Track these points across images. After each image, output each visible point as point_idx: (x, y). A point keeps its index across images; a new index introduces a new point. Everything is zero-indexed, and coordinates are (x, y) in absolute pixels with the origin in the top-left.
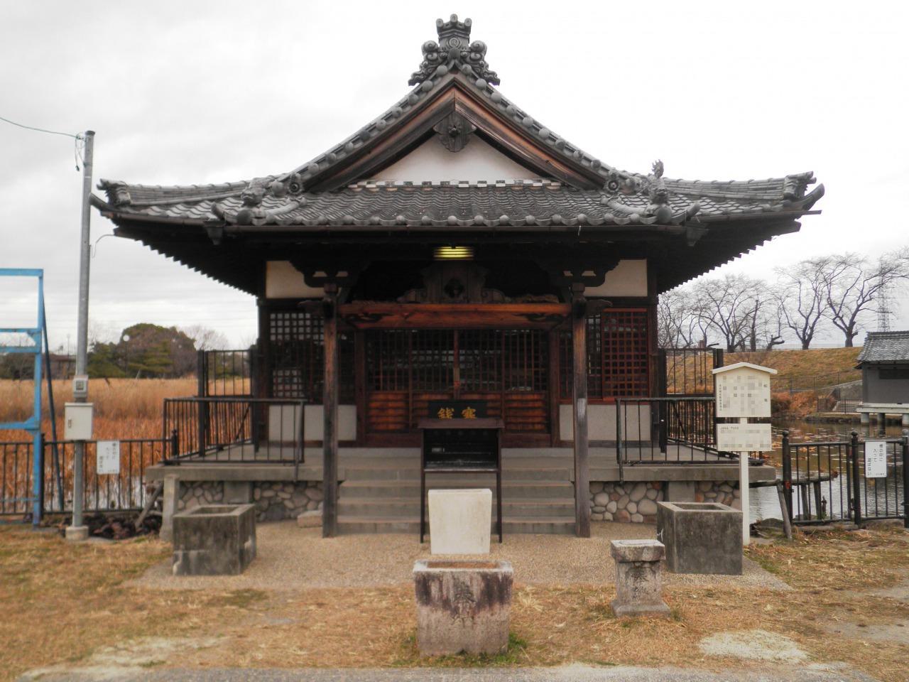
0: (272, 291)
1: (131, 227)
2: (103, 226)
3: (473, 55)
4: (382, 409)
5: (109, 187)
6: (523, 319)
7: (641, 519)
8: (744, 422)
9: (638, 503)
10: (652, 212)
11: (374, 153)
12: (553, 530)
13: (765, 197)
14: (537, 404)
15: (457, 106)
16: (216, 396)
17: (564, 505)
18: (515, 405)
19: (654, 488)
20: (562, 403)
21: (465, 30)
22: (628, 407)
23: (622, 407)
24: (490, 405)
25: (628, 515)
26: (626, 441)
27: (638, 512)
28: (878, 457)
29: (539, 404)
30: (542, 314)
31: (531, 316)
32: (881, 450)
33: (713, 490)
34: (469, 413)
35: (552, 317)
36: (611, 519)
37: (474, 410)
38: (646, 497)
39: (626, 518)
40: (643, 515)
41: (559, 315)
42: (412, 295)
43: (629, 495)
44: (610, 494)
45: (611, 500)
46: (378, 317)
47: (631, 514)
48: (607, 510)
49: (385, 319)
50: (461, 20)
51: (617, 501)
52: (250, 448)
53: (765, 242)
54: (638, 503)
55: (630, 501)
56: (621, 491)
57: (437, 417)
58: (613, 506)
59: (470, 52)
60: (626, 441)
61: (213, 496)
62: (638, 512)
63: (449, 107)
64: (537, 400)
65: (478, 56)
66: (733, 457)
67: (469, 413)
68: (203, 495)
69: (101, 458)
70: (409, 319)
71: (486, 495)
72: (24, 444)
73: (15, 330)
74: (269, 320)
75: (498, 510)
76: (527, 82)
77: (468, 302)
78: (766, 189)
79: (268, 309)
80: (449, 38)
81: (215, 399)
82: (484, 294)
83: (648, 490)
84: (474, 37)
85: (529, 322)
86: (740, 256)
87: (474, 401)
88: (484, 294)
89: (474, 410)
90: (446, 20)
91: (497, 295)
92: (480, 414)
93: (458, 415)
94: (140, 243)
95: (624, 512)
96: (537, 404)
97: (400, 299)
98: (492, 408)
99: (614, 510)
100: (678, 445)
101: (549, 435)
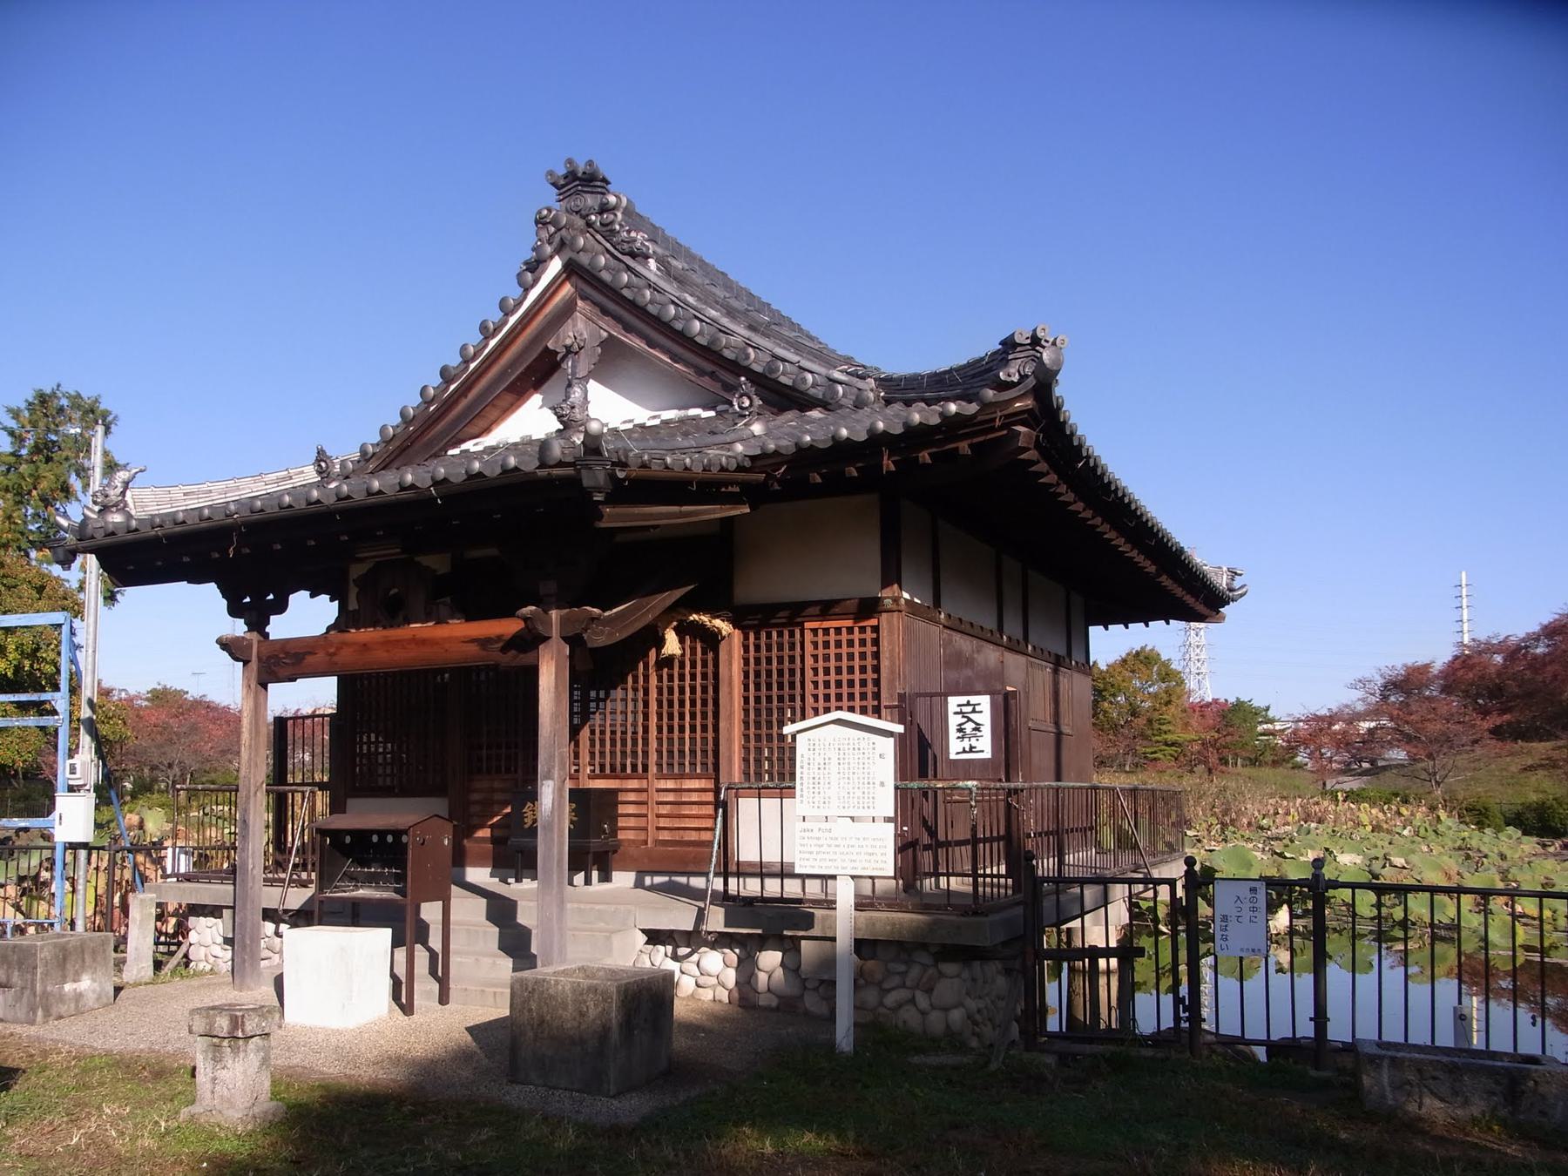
30: (499, 638)
90: (561, 171)
94: (181, 588)
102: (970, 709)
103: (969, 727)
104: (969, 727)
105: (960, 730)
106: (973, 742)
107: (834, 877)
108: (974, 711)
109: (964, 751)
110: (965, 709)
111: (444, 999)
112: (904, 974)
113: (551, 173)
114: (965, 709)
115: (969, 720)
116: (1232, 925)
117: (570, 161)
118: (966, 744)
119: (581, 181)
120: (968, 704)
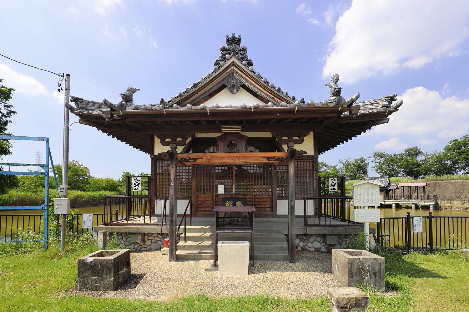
0: (156, 153)
1: (88, 119)
2: (74, 118)
3: (241, 52)
4: (204, 201)
5: (76, 100)
6: (265, 161)
7: (314, 250)
8: (367, 208)
9: (312, 243)
10: (332, 101)
11: (200, 93)
12: (277, 259)
13: (372, 108)
14: (267, 200)
15: (235, 75)
16: (134, 195)
17: (282, 246)
18: (258, 200)
19: (319, 236)
20: (278, 199)
21: (238, 41)
22: (309, 200)
23: (307, 201)
24: (248, 200)
25: (308, 248)
26: (308, 215)
27: (312, 247)
28: (419, 223)
29: (269, 200)
30: (274, 157)
31: (269, 158)
32: (420, 221)
33: (345, 237)
34: (239, 203)
35: (278, 159)
36: (301, 250)
37: (241, 202)
38: (316, 240)
39: (307, 249)
40: (315, 248)
41: (282, 158)
42: (212, 149)
43: (308, 239)
44: (300, 239)
45: (300, 242)
46: (195, 160)
47: (309, 248)
48: (299, 246)
49: (199, 161)
50: (237, 36)
51: (303, 242)
52: (148, 217)
53: (353, 138)
54: (312, 243)
55: (309, 242)
56: (305, 238)
57: (225, 205)
58: (301, 244)
59: (240, 51)
60: (308, 215)
61: (127, 239)
62: (312, 247)
63: (232, 73)
64: (267, 198)
65: (244, 52)
66: (361, 225)
67: (239, 203)
68: (122, 238)
69: (84, 221)
70: (210, 160)
71: (246, 244)
72: (295, 189)
73: (28, 165)
74: (156, 164)
75: (252, 249)
76: (265, 65)
77: (239, 152)
78: (372, 104)
79: (156, 159)
80: (231, 44)
81: (133, 197)
82: (246, 148)
83: (317, 237)
84: (242, 45)
85: (268, 161)
86: (343, 143)
87: (241, 198)
88: (246, 148)
89: (241, 202)
90: (230, 36)
91: (252, 149)
92: (244, 204)
93: (234, 205)
94: (95, 129)
95: (307, 247)
96: (267, 200)
97: (206, 151)
98: (249, 201)
99: (302, 246)
100: (325, 217)
101: (272, 212)
102: (137, 180)
103: (137, 184)
104: (137, 184)
105: (332, 184)
106: (334, 188)
107: (380, 218)
108: (138, 181)
109: (136, 189)
110: (136, 180)
111: (207, 270)
112: (346, 241)
113: (227, 36)
114: (136, 180)
115: (137, 182)
116: (86, 222)
117: (233, 34)
118: (136, 187)
119: (234, 41)
120: (137, 179)
